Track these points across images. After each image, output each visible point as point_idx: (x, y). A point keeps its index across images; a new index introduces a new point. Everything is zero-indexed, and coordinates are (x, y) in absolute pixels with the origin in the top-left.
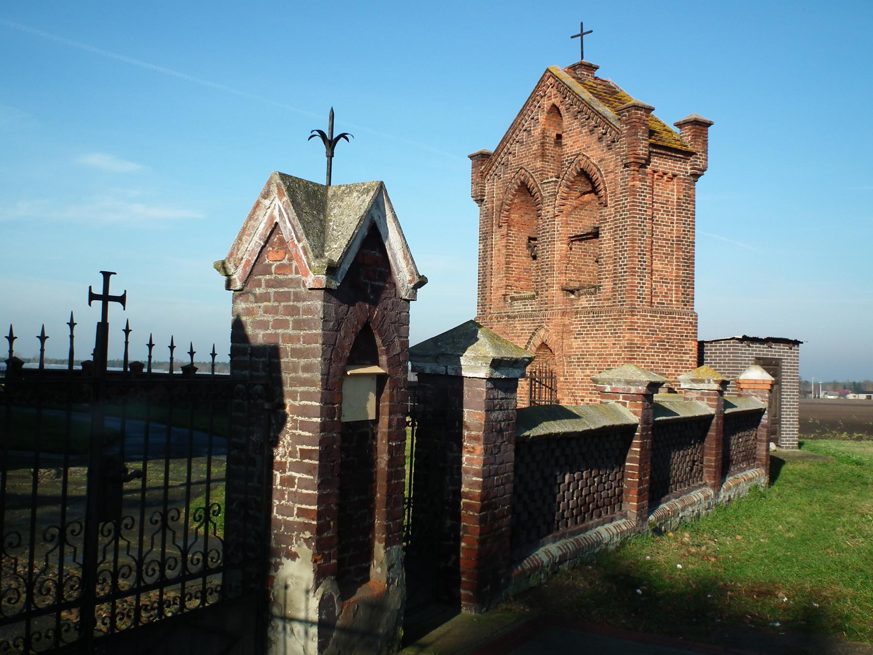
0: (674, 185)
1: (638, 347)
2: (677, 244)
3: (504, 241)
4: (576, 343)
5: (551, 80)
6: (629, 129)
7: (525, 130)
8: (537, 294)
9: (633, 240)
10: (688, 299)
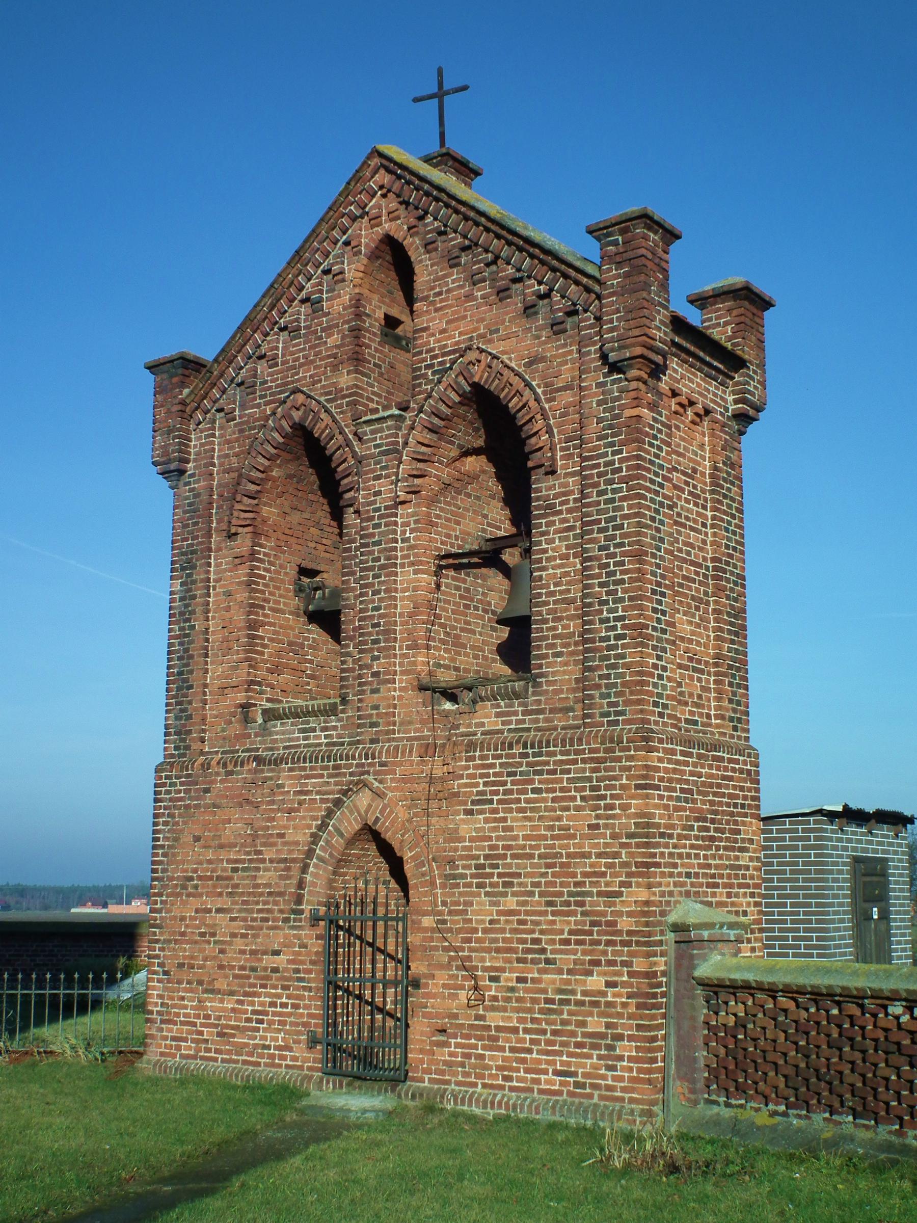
0: (704, 435)
1: (662, 835)
2: (714, 578)
3: (243, 571)
4: (468, 827)
5: (383, 177)
6: (627, 275)
7: (303, 301)
8: (344, 701)
9: (639, 556)
10: (740, 720)
